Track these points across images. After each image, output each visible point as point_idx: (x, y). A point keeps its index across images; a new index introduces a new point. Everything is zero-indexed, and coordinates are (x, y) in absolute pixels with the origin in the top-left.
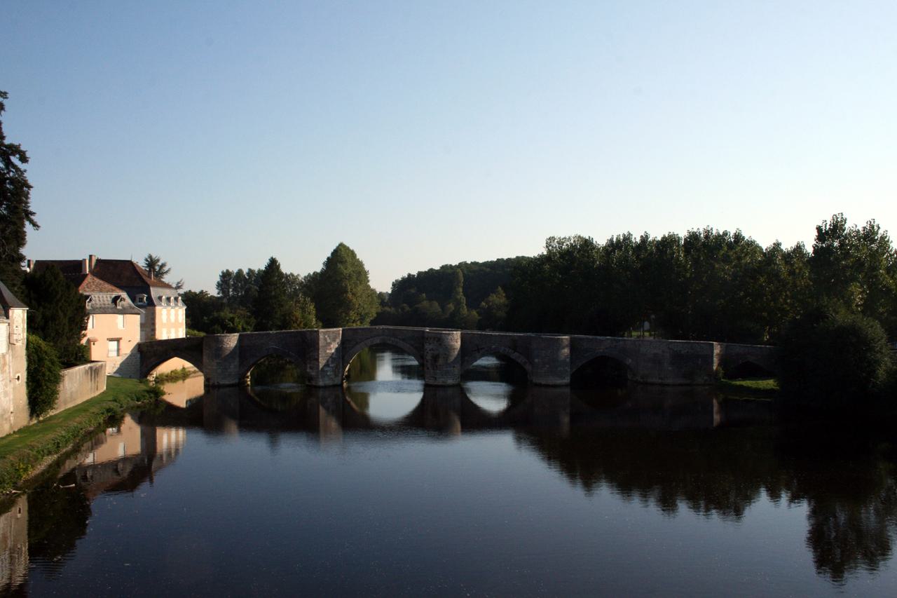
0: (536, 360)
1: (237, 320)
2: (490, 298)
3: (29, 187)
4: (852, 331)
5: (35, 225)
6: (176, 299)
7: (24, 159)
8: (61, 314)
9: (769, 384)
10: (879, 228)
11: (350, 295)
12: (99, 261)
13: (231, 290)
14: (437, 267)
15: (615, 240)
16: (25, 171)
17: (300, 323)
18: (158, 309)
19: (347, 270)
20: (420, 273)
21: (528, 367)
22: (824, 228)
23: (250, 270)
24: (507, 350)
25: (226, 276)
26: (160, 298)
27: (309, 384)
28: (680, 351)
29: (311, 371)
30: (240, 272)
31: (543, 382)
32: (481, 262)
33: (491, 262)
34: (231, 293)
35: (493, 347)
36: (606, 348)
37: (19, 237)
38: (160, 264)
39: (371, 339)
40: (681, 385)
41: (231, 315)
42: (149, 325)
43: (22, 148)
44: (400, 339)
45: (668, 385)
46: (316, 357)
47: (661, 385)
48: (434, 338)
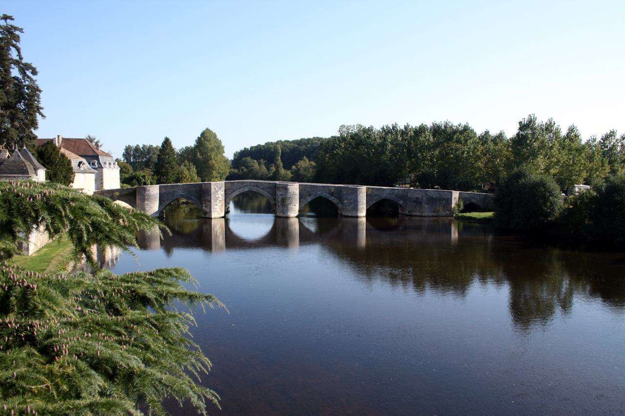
0: (345, 201)
1: (147, 177)
2: (299, 163)
3: (40, 91)
4: (542, 184)
5: (43, 116)
6: (114, 164)
7: (34, 72)
8: (59, 173)
9: (489, 214)
10: (555, 123)
11: (213, 161)
12: (64, 139)
13: (132, 158)
14: (263, 144)
15: (385, 128)
16: (36, 81)
17: (189, 178)
18: (104, 170)
19: (209, 145)
20: (252, 148)
21: (340, 206)
22: (523, 122)
23: (144, 145)
24: (327, 195)
25: (128, 149)
26: (105, 163)
27: (205, 216)
28: (433, 196)
29: (206, 208)
30: (137, 147)
31: (350, 215)
32: (290, 140)
33: (297, 140)
34: (132, 160)
35: (319, 193)
36: (388, 194)
37: (34, 124)
38: (95, 141)
39: (243, 188)
40: (432, 216)
41: (143, 174)
42: (99, 180)
43: (34, 66)
44: (261, 188)
45: (425, 216)
46: (209, 200)
47: (421, 216)
48: (283, 188)
